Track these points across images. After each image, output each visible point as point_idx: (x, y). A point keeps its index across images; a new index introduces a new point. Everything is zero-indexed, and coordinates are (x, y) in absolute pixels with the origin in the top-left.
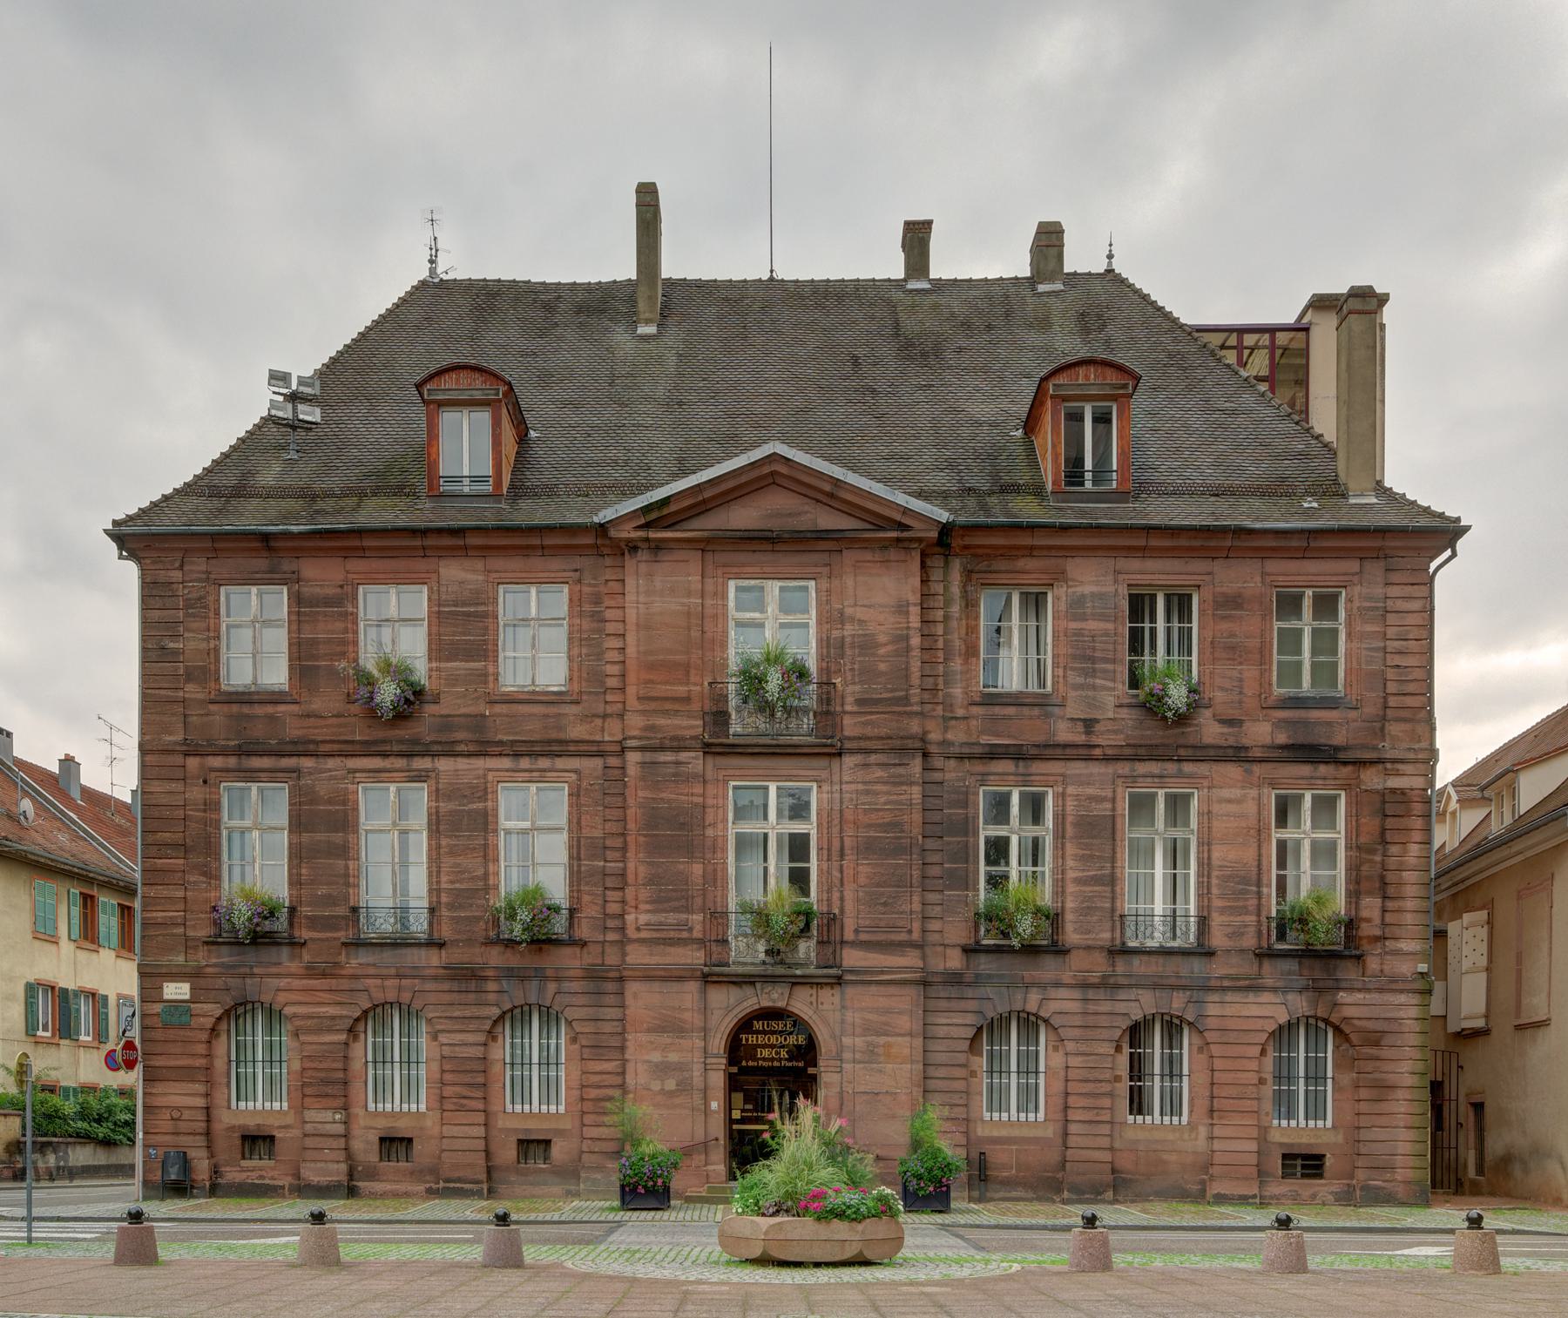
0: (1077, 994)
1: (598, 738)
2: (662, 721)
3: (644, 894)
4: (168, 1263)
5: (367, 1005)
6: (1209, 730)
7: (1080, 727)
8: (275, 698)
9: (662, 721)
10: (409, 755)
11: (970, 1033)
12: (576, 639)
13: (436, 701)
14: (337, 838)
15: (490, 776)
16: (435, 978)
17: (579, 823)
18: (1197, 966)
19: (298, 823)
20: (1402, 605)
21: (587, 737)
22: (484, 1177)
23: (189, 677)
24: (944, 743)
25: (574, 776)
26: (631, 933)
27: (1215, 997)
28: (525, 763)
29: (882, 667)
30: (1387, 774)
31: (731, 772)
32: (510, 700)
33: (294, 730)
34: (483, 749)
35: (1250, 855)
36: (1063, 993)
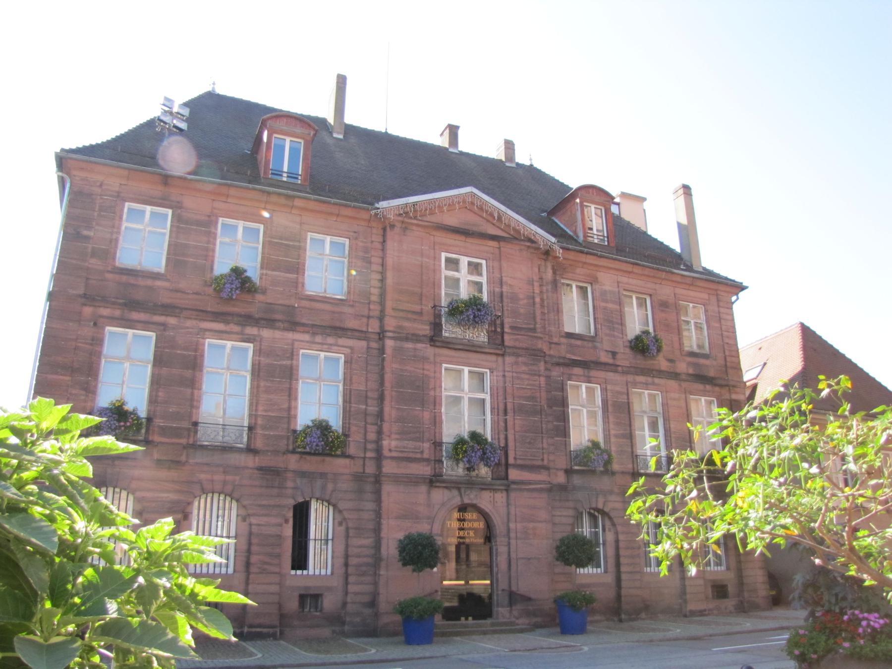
1: (364, 329)
2: (406, 324)
6: (662, 363)
7: (610, 355)
8: (156, 276)
10: (243, 325)
13: (264, 292)
14: (188, 373)
15: (296, 343)
17: (351, 380)
19: (159, 361)
21: (357, 328)
22: (277, 623)
23: (94, 254)
25: (348, 351)
26: (386, 453)
28: (318, 339)
29: (522, 311)
32: (311, 299)
33: (165, 298)
34: (293, 325)
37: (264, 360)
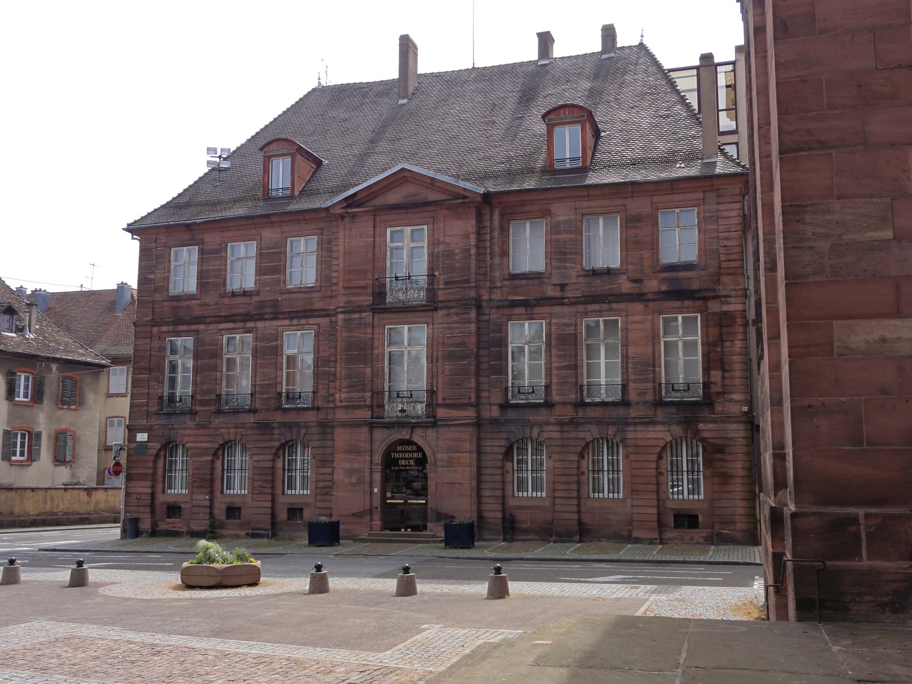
0: (557, 428)
2: (354, 299)
3: (345, 383)
4: (25, 582)
5: (221, 442)
7: (558, 289)
8: (191, 297)
9: (354, 299)
10: (245, 321)
11: (503, 450)
12: (320, 261)
14: (213, 361)
16: (252, 428)
18: (621, 411)
20: (726, 214)
22: (269, 527)
24: (490, 300)
27: (631, 428)
28: (295, 322)
29: (458, 265)
30: (722, 303)
31: (385, 321)
32: (290, 292)
33: (197, 312)
34: (276, 316)
35: (649, 350)
36: (551, 428)
37: (259, 344)
